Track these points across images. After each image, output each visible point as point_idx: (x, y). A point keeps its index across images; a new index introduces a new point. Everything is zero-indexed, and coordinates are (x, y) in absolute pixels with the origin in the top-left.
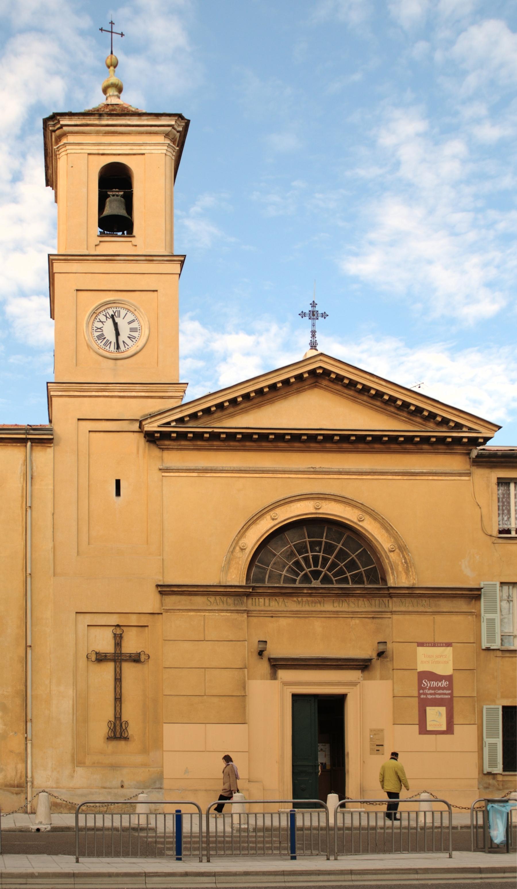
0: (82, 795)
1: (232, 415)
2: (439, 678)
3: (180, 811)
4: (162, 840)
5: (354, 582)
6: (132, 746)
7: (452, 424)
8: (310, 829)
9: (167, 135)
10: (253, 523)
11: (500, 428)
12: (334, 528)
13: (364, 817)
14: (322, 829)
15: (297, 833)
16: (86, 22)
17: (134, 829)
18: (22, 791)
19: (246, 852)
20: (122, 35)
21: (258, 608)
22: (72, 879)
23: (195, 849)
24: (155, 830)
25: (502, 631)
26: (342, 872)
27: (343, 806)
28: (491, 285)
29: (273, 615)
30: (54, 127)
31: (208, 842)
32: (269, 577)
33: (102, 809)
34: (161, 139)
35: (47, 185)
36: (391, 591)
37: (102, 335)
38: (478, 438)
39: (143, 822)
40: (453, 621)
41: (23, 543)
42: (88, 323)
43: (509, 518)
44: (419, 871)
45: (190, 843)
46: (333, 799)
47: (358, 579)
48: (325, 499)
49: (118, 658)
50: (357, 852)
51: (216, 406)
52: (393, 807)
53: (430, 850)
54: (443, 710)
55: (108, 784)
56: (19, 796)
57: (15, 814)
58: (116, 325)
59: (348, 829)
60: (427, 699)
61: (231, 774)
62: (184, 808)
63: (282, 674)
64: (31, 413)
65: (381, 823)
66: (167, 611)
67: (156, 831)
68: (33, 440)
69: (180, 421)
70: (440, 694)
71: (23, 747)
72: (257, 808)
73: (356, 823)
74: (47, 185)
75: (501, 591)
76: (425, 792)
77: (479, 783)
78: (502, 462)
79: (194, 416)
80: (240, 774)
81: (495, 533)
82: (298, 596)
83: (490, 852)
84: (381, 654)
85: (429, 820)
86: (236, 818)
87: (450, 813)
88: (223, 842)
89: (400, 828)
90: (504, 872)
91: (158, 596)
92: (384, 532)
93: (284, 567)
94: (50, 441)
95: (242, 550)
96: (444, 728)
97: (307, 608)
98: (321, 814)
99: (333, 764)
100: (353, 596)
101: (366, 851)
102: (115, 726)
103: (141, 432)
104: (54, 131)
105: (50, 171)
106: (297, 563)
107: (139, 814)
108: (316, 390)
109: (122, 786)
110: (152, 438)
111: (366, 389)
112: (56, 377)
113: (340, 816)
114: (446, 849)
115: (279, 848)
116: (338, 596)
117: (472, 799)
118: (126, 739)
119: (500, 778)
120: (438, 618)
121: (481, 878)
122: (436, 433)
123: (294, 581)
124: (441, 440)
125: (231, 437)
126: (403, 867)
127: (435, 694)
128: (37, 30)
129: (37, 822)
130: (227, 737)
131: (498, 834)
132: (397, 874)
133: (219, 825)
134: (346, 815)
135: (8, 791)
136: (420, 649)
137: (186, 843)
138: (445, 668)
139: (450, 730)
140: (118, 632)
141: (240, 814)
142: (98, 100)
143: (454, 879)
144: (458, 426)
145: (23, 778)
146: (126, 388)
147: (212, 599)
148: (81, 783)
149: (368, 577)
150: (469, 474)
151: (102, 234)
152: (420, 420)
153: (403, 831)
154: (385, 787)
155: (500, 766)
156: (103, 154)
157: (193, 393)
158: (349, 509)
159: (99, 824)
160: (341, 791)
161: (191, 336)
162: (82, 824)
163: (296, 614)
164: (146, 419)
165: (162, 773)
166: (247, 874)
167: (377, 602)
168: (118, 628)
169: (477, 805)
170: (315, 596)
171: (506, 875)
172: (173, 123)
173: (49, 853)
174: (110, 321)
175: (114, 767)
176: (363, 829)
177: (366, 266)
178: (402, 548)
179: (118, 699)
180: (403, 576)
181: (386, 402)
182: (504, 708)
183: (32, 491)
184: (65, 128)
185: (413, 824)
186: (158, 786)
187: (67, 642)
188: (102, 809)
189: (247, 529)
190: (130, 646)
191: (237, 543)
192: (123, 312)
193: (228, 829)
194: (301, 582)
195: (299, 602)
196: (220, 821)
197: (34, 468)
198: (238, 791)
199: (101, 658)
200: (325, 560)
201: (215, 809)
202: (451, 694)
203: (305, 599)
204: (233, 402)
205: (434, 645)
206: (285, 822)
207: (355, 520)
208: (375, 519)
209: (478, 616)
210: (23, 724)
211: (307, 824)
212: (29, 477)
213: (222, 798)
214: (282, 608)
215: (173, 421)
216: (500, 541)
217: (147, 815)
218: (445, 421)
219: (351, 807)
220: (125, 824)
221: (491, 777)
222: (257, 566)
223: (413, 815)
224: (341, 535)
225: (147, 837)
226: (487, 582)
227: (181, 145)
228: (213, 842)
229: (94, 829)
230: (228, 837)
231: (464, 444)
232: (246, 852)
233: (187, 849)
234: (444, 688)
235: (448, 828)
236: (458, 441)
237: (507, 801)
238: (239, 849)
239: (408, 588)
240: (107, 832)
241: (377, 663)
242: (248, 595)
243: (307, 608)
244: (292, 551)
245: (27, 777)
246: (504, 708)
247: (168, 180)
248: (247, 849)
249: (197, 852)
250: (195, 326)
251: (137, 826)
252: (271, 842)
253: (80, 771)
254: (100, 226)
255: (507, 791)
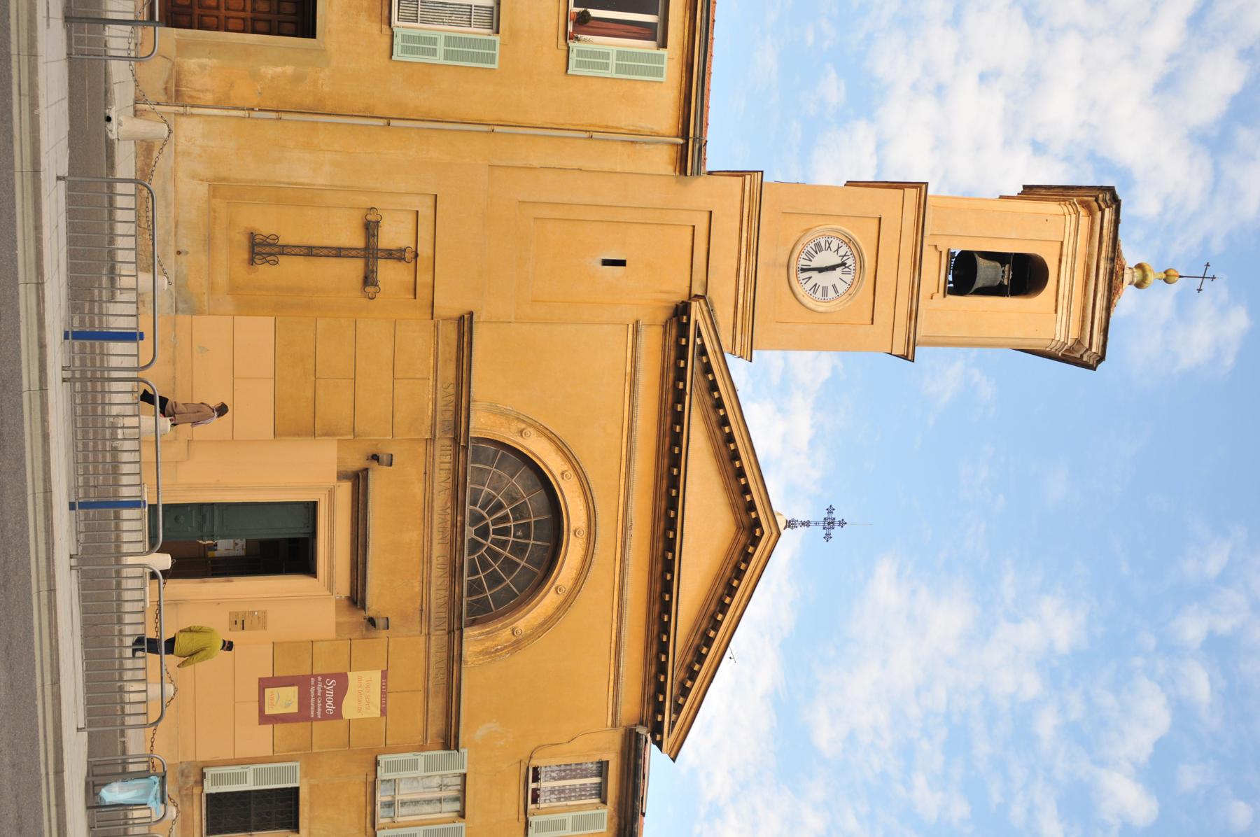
0: (164, 190)
1: (706, 419)
2: (338, 702)
3: (142, 338)
4: (96, 311)
5: (470, 584)
6: (241, 270)
7: (681, 701)
8: (118, 529)
9: (1079, 342)
10: (559, 448)
11: (674, 760)
12: (547, 555)
13: (138, 606)
14: (118, 547)
15: (112, 511)
16: (1217, 246)
17: (112, 269)
18: (170, 98)
19: (79, 437)
20: (1199, 290)
21: (437, 453)
22: (29, 169)
23: (82, 360)
24: (112, 299)
25: (401, 779)
26: (51, 577)
27: (153, 576)
28: (851, 738)
29: (428, 475)
30: (1102, 200)
31: (93, 380)
32: (481, 469)
33: (144, 220)
34: (1074, 333)
35: (1025, 187)
36: (457, 633)
37: (821, 250)
38: (662, 733)
39: (124, 282)
40: (416, 714)
41: (539, 123)
42: (837, 231)
43: (554, 779)
44: (56, 687)
45: (93, 352)
46: (164, 561)
47: (475, 588)
48: (588, 543)
49: (371, 253)
50: (84, 598)
51: (720, 399)
52: (153, 646)
53: (89, 701)
54: (294, 708)
55: (182, 231)
56: (162, 92)
57: (133, 84)
58: (833, 268)
59: (119, 585)
60: (309, 686)
61: (199, 414)
62: (146, 344)
63: (345, 488)
64: (723, 147)
65: (128, 630)
66: (436, 327)
67: (109, 301)
68: (685, 147)
69: (703, 351)
70: (316, 703)
71: (239, 104)
72: (148, 453)
73: (127, 595)
74: (1025, 187)
75: (454, 776)
76: (176, 690)
77: (190, 763)
78: (629, 765)
79: (708, 369)
80: (199, 429)
81: (534, 763)
82: (452, 509)
83: (87, 784)
84: (372, 622)
85: (134, 697)
86: (133, 421)
87: (144, 726)
88: (94, 402)
89: (121, 658)
90: (57, 805)
91: (457, 314)
92: (541, 620)
93: (495, 489)
94: (683, 171)
95: (521, 432)
96: (268, 711)
97: (437, 520)
98: (140, 545)
99: (216, 561)
100: (452, 583)
101: (85, 610)
102: (270, 245)
103: (690, 298)
104: (1097, 200)
105: (1043, 192)
106: (500, 506)
107: (136, 276)
108: (733, 529)
109: (179, 253)
110: (681, 311)
111: (731, 591)
112: (769, 184)
113: (138, 572)
114: (90, 723)
115: (86, 484)
116: (453, 562)
117: (165, 754)
118: (252, 261)
119: (197, 790)
120: (420, 696)
121: (47, 774)
122: (669, 684)
123: (474, 503)
124: (661, 688)
125: (678, 418)
126: (61, 664)
127: (316, 696)
128: (1216, 185)
129: (121, 118)
130: (254, 408)
131: (114, 793)
132: (51, 656)
133: (121, 396)
134: (140, 580)
135: (170, 75)
136: (377, 675)
137: (92, 347)
138: (350, 709)
139: (264, 719)
140: (408, 256)
141: (138, 427)
142: (1130, 257)
143: (45, 736)
144: (678, 709)
145: (189, 101)
146: (749, 279)
147: (451, 390)
148: (182, 191)
149: (478, 601)
150: (614, 725)
151: (951, 255)
152: (688, 660)
153: (117, 662)
154: (182, 635)
155: (214, 790)
156: (1060, 261)
157: (737, 366)
158: (574, 573)
159: (120, 215)
160: (179, 571)
161: (814, 366)
162: (120, 188)
163: (429, 505)
164: (707, 305)
165: (200, 312)
166: (46, 437)
167: (443, 615)
168: (412, 255)
169: (156, 762)
170: (452, 531)
171: (53, 809)
172: (1094, 350)
173: (70, 134)
174: (838, 261)
175: (209, 242)
176: (119, 606)
177: (885, 588)
178: (517, 645)
179: (310, 252)
180: (478, 648)
181: (713, 617)
182: (297, 789)
183: (657, 143)
184: (1099, 214)
185: (128, 675)
186: (181, 306)
187: (400, 181)
188: (144, 220)
189: (550, 439)
190: (388, 272)
191: (531, 425)
192: (848, 278)
193: (115, 410)
194: (471, 511)
195: (444, 510)
196: (128, 398)
197: (646, 147)
198: (174, 425)
199: (370, 228)
200: (503, 544)
201: (145, 392)
202: (315, 719)
203: (449, 517)
204: (724, 421)
205: (384, 693)
206: (127, 493)
207: (557, 583)
208: (558, 609)
209: (422, 748)
210: (273, 106)
211: (126, 526)
212: (635, 139)
213: (164, 401)
214: (437, 487)
215: (702, 340)
216: (523, 770)
217: (136, 289)
218: (685, 692)
219: (151, 586)
220: (121, 256)
221: (198, 778)
222: (496, 453)
223: (140, 675)
224: (538, 565)
225: (100, 287)
226: (466, 758)
227: (1066, 359)
228: (94, 387)
229: (112, 207)
230: (103, 409)
231: (654, 717)
232: (79, 437)
233: (83, 348)
234: (323, 708)
235: (123, 724)
236: (659, 709)
237: (163, 802)
238: (85, 426)
239: (461, 655)
240: (106, 226)
241: (359, 617)
242: (456, 440)
243: (437, 520)
244: (517, 500)
245: (193, 106)
246: (297, 789)
247: (1019, 342)
248: (85, 438)
249: (77, 363)
250: (826, 373)
251: (117, 272)
252: (96, 473)
253: (203, 189)
254: (963, 253)
255: (178, 801)
